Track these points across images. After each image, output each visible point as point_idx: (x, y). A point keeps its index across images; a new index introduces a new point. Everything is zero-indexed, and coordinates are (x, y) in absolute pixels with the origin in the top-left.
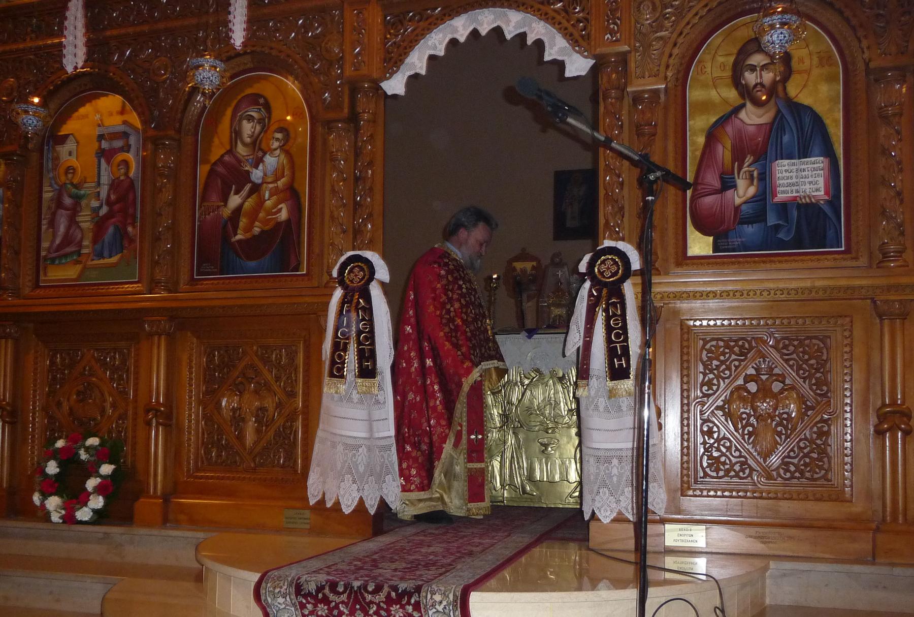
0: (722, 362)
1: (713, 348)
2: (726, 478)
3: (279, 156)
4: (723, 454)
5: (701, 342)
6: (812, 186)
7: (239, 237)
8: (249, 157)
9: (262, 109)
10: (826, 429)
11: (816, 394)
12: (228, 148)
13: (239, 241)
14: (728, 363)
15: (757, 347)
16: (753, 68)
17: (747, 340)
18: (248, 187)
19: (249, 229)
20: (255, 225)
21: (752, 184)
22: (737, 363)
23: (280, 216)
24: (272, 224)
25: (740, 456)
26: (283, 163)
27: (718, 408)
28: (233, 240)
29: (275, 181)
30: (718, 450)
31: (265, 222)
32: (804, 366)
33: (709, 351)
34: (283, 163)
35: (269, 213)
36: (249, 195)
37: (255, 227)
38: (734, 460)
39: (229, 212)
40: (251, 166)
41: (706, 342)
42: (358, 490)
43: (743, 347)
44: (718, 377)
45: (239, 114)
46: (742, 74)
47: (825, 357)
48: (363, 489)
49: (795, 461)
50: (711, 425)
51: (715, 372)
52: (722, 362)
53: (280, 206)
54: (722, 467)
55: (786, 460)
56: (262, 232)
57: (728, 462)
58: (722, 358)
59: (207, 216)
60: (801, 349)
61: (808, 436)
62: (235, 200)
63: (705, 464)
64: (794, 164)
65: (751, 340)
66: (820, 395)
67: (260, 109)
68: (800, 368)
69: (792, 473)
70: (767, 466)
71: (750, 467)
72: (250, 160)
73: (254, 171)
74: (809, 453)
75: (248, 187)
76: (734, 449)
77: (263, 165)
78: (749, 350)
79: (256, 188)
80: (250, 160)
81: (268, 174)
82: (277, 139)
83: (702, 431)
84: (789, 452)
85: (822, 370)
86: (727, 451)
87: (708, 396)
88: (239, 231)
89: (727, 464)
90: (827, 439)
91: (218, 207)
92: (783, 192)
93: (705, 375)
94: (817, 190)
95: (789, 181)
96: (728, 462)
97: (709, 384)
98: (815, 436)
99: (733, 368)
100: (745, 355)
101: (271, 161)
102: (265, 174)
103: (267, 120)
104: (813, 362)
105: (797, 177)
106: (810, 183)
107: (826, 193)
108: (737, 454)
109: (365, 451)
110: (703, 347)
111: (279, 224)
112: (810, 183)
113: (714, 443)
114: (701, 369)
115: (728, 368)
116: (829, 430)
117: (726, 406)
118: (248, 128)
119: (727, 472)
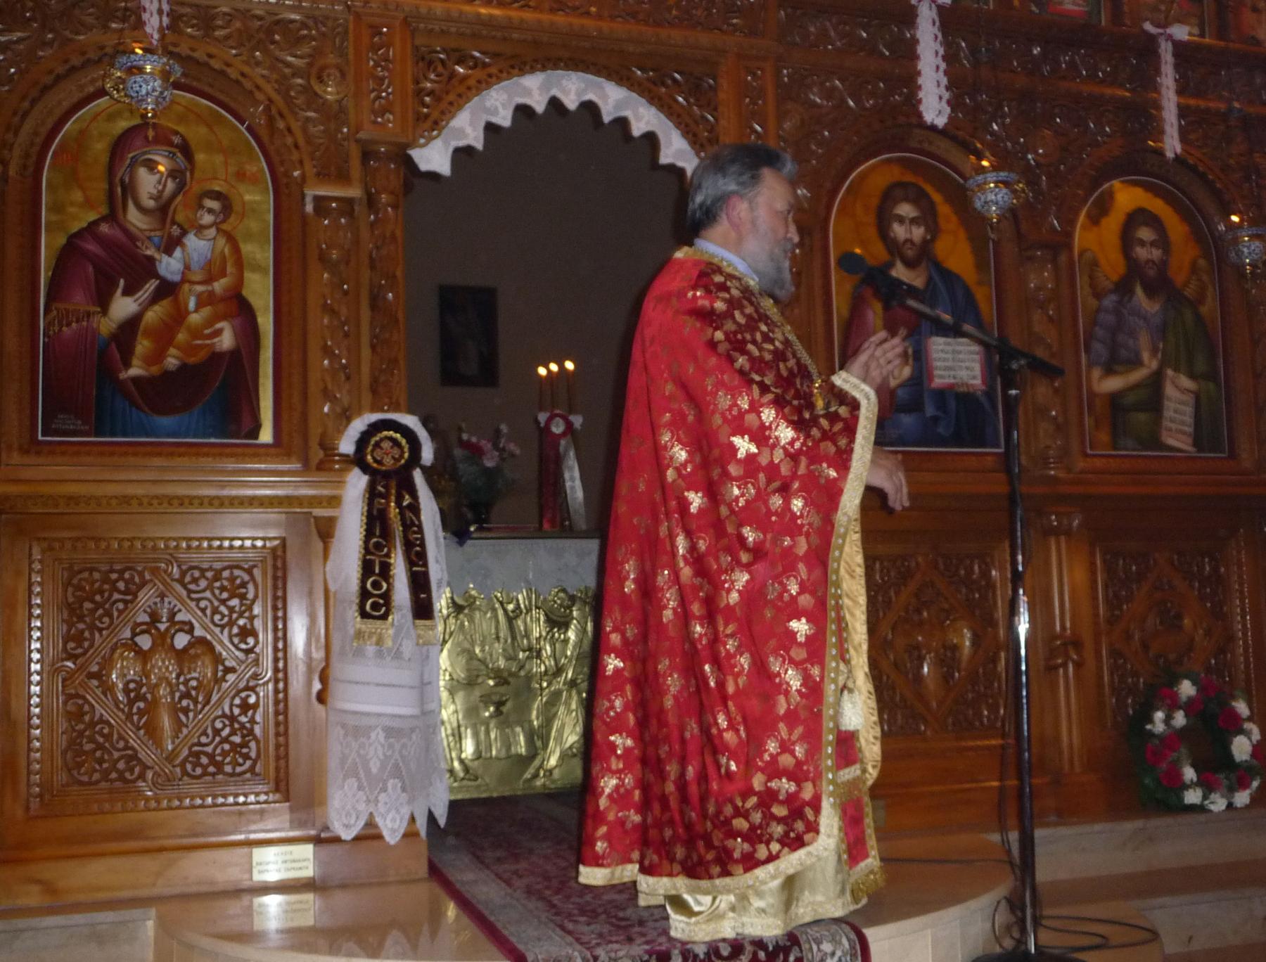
0: (226, 740)
1: (241, 760)
2: (218, 567)
3: (214, 238)
4: (223, 602)
5: (257, 769)
6: (969, 372)
7: (134, 371)
8: (153, 234)
9: (179, 155)
10: (71, 645)
11: (84, 698)
12: (104, 210)
13: (136, 380)
14: (107, 606)
15: (174, 766)
16: (901, 220)
17: (189, 775)
18: (151, 286)
19: (157, 356)
20: (169, 352)
21: (906, 363)
22: (204, 740)
23: (221, 341)
24: (202, 356)
25: (198, 600)
26: (222, 252)
27: (232, 670)
28: (123, 375)
29: (209, 280)
30: (231, 610)
31: (189, 349)
32: (101, 740)
33: (246, 757)
34: (222, 252)
35: (196, 333)
36: (156, 298)
37: (170, 356)
38: (208, 594)
39: (114, 326)
40: (158, 249)
41: (252, 769)
42: (368, 801)
43: (197, 764)
44: (233, 719)
45: (131, 155)
46: (889, 226)
47: (69, 755)
48: (377, 801)
49: (116, 596)
50: (243, 646)
51: (236, 726)
52: (226, 740)
53: (219, 325)
54: (226, 583)
55: (129, 598)
56: (183, 367)
57: (217, 592)
58: (227, 747)
59: (65, 329)
60: (105, 765)
61: (97, 635)
62: (123, 306)
63: (251, 587)
64: (949, 344)
65: (182, 776)
66: (77, 696)
67: (174, 154)
68: (108, 737)
69: (121, 578)
70: (155, 585)
71: (184, 586)
72: (156, 240)
73: (165, 258)
74: (96, 609)
75: (151, 286)
76: (208, 612)
77: (183, 251)
78: (185, 760)
79: (167, 289)
80: (156, 240)
81: (192, 268)
82: (210, 211)
83: (255, 635)
84: (126, 608)
85: (74, 734)
86: (218, 607)
87: (247, 688)
88: (135, 362)
89: (218, 588)
90: (69, 631)
91: (88, 315)
92: (942, 377)
93: (252, 721)
94: (974, 378)
95: (946, 364)
96: (217, 592)
97: (245, 707)
98: (87, 634)
99: (209, 731)
100: (191, 754)
101: (197, 246)
102: (187, 267)
103: (188, 174)
104: (88, 747)
105: (954, 360)
106: (967, 368)
107: (984, 382)
108: (203, 604)
109: (382, 740)
110: (255, 762)
111: (216, 357)
112: (967, 368)
113: (237, 619)
114: (258, 730)
115: (217, 732)
116: (65, 644)
117: (220, 674)
118: (147, 183)
119: (218, 577)
